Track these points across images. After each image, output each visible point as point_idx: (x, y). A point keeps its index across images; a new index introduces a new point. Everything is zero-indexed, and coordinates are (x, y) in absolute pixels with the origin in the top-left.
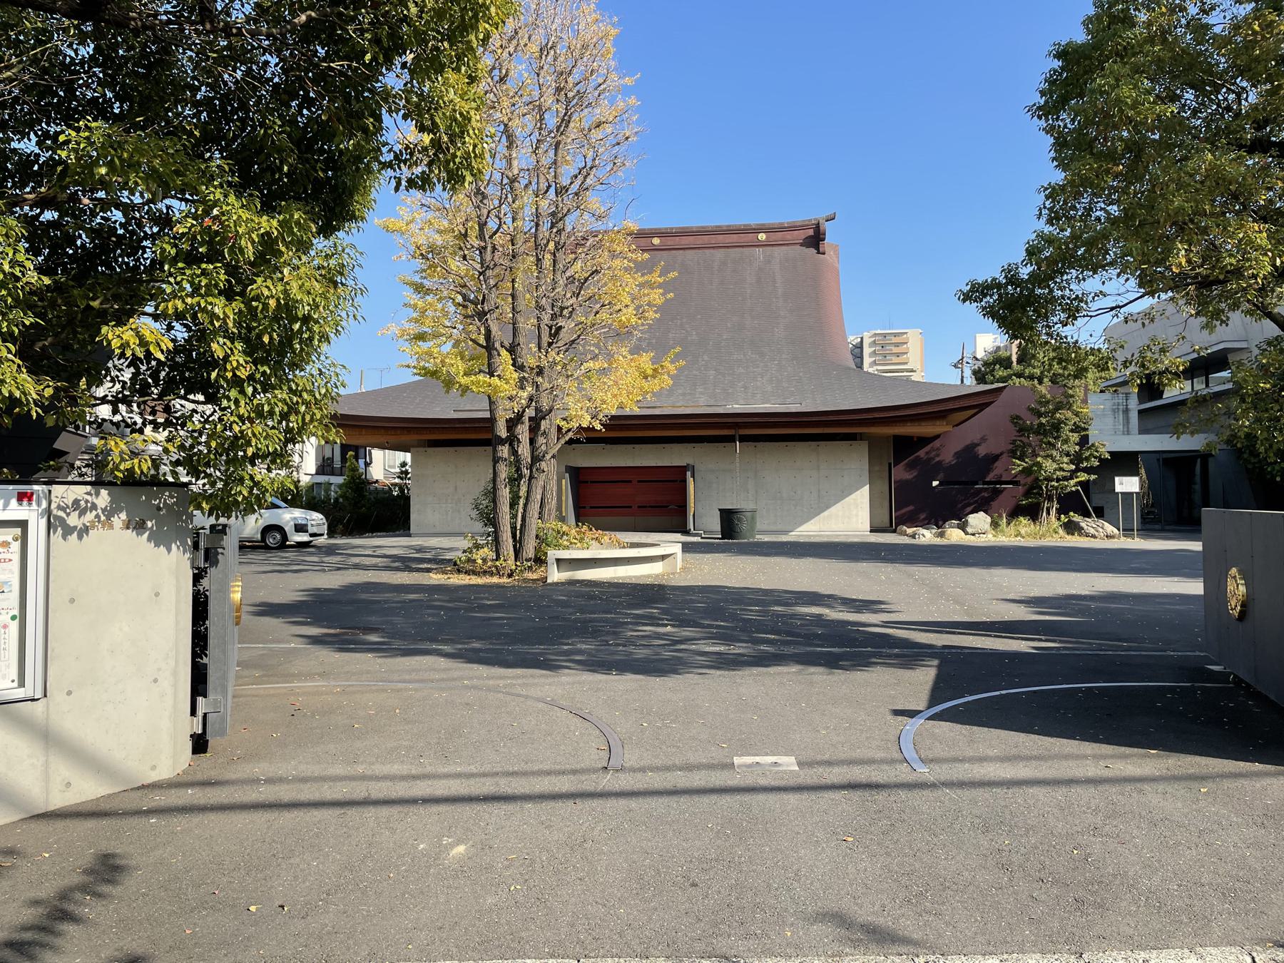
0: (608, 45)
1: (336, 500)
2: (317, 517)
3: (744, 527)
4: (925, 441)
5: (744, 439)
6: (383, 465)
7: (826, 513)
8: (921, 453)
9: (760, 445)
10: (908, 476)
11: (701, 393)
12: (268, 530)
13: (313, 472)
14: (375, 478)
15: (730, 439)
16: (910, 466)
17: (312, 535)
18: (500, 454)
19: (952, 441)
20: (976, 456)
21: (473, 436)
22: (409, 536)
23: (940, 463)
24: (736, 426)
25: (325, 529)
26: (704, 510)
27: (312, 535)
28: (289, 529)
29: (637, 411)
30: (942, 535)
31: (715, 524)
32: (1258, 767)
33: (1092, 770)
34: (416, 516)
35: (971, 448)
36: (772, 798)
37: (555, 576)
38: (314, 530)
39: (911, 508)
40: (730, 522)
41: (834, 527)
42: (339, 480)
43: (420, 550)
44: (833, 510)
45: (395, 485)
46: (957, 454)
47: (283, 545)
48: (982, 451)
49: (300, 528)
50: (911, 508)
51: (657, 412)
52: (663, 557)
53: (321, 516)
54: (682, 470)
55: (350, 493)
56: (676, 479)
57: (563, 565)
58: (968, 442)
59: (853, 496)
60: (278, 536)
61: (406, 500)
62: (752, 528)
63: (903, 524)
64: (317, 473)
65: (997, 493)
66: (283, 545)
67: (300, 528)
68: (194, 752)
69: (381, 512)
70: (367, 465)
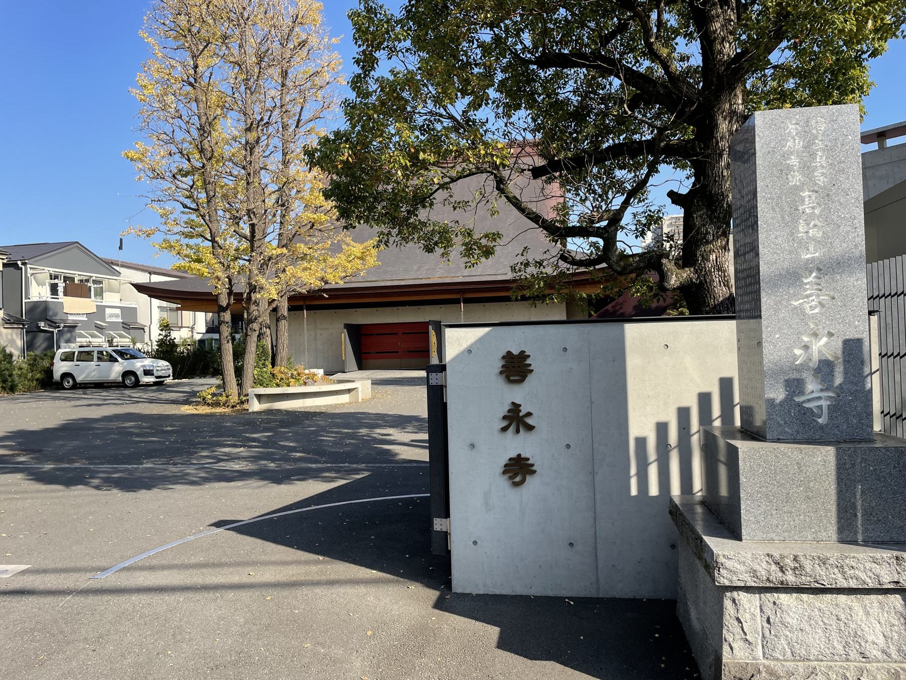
9: (487, 304)
11: (441, 268)
12: (126, 374)
13: (204, 331)
15: (456, 302)
17: (157, 377)
18: (222, 319)
21: (473, 286)
27: (157, 377)
28: (140, 373)
29: (341, 284)
32: (374, 573)
33: (269, 575)
36: (144, 598)
37: (256, 406)
47: (137, 384)
49: (147, 373)
51: (403, 283)
52: (349, 391)
53: (167, 364)
57: (263, 399)
60: (133, 379)
64: (207, 332)
66: (137, 384)
67: (147, 373)
68: (738, 537)
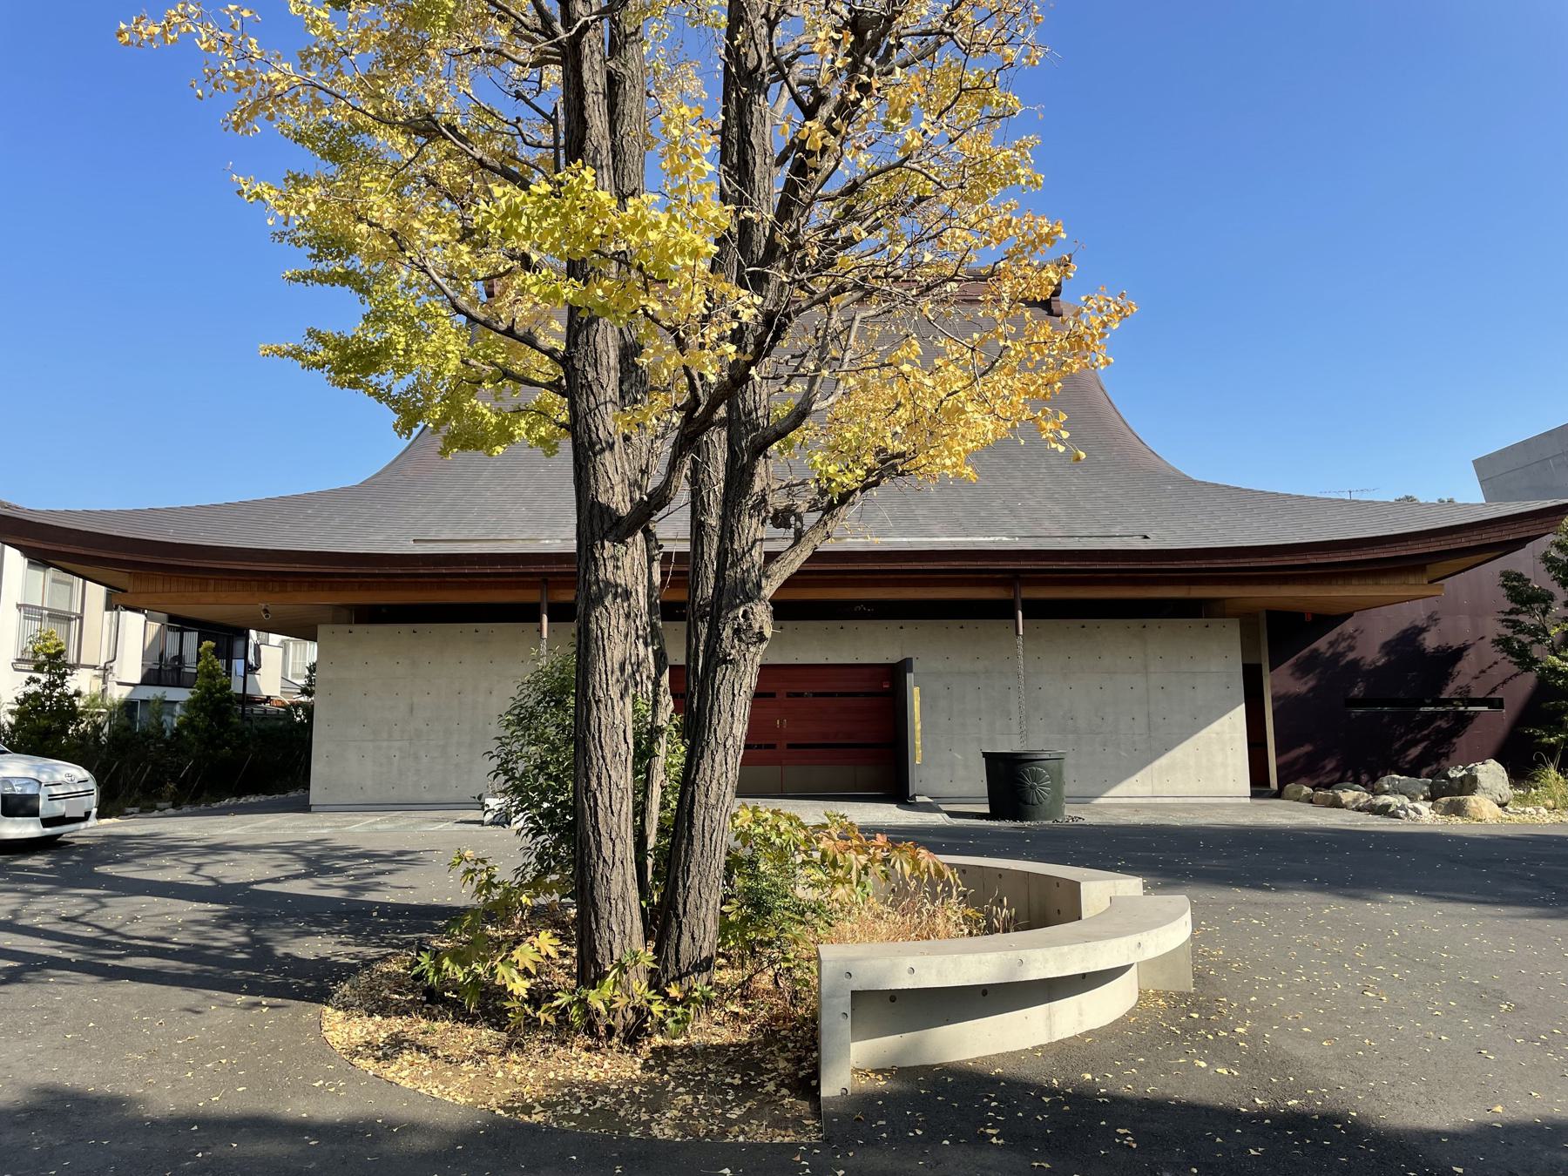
0: (604, 196)
1: (177, 733)
2: (71, 775)
3: (1044, 790)
4: (1327, 620)
5: (1036, 611)
6: (278, 667)
7: (1163, 761)
8: (1322, 644)
10: (1300, 687)
13: (138, 680)
14: (265, 693)
15: (1002, 611)
16: (1302, 669)
19: (1376, 623)
20: (1420, 652)
22: (304, 807)
23: (1355, 663)
24: (1013, 579)
25: (92, 802)
26: (947, 761)
27: (47, 822)
30: (1458, 809)
31: (975, 781)
34: (327, 763)
35: (1411, 636)
38: (60, 808)
39: (1307, 748)
40: (1011, 782)
41: (1181, 789)
42: (182, 695)
43: (318, 862)
44: (1178, 753)
45: (297, 705)
46: (1388, 647)
48: (1430, 641)
50: (1307, 748)
54: (903, 667)
55: (201, 721)
56: (885, 690)
58: (1406, 625)
59: (1215, 726)
61: (307, 727)
62: (1058, 799)
63: (1295, 780)
64: (146, 681)
65: (1463, 721)
69: (260, 758)
70: (251, 669)
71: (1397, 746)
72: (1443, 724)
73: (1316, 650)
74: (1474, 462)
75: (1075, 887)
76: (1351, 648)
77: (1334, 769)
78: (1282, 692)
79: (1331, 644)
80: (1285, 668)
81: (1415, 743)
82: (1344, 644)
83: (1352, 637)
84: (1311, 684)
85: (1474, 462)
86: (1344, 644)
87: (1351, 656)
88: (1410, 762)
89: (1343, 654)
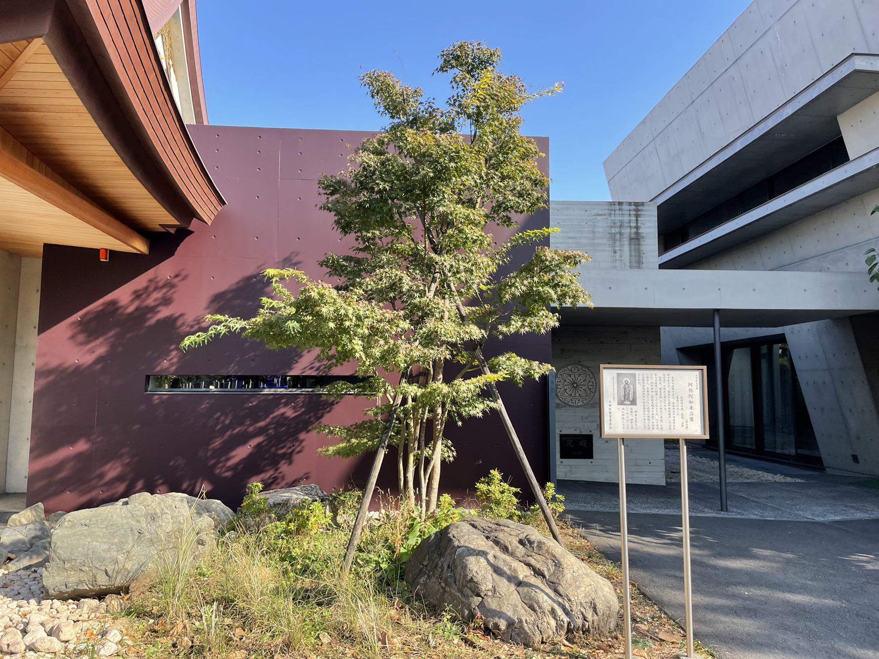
7: (577, 432)
16: (90, 329)
39: (82, 446)
50: (82, 446)
71: (217, 443)
72: (289, 412)
73: (113, 303)
74: (591, 457)
75: (561, 436)
76: (166, 301)
77: (119, 479)
78: (54, 363)
79: (137, 295)
80: (63, 329)
81: (243, 439)
82: (157, 295)
83: (169, 285)
84: (101, 351)
85: (591, 457)
86: (157, 295)
87: (164, 313)
88: (234, 468)
89: (153, 310)
